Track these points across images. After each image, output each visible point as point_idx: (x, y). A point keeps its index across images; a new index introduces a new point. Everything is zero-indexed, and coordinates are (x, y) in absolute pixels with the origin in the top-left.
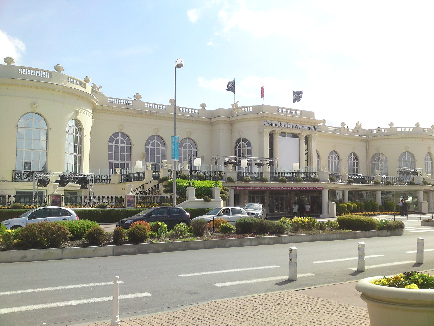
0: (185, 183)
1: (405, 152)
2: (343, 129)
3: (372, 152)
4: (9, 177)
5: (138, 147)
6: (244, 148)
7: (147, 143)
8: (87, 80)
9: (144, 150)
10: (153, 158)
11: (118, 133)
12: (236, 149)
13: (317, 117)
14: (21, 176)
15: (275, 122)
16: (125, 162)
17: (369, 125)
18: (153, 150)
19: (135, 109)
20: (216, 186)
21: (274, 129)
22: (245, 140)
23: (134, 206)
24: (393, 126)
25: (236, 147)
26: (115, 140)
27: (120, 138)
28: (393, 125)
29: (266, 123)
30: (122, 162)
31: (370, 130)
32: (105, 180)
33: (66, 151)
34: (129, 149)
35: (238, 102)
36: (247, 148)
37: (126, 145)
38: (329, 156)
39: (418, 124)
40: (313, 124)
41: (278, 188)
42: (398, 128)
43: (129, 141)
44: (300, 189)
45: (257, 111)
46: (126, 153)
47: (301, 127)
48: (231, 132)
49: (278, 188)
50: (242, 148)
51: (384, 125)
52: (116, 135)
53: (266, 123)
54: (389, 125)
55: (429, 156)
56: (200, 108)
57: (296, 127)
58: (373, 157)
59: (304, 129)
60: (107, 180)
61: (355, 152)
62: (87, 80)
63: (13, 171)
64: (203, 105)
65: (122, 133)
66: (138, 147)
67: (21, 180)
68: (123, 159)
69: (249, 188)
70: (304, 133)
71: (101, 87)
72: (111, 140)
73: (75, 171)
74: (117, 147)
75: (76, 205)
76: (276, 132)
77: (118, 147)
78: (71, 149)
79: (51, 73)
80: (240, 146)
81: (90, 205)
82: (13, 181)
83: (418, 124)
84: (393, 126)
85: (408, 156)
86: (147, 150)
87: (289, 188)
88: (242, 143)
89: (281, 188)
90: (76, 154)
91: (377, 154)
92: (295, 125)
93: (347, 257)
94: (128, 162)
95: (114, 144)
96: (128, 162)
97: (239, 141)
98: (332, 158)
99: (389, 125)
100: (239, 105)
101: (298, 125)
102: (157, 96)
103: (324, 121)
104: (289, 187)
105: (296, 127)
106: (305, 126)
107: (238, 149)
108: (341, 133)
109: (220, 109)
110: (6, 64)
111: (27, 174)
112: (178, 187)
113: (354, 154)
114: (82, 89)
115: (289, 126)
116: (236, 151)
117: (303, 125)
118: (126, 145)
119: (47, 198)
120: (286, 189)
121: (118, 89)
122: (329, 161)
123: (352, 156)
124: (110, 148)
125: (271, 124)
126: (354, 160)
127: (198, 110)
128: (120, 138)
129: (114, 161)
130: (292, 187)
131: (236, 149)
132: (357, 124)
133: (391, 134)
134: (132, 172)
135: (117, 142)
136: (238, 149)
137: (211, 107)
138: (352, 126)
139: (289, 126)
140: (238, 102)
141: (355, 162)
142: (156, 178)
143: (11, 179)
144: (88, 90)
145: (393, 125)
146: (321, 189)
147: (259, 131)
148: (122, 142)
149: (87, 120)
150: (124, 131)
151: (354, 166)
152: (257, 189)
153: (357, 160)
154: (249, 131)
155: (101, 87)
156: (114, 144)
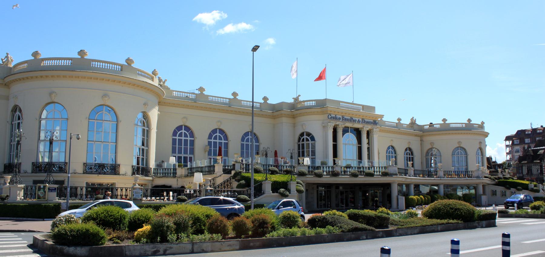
0: (259, 177)
2: (399, 125)
3: (427, 147)
4: (80, 169)
5: (201, 141)
6: (308, 142)
7: (210, 137)
8: (154, 73)
9: (207, 144)
10: (180, 149)
11: (216, 129)
13: (378, 112)
14: (91, 168)
15: (338, 116)
16: (188, 156)
17: (423, 121)
18: (180, 141)
19: (199, 101)
20: (266, 179)
21: (337, 123)
22: (309, 134)
23: (197, 196)
24: (446, 122)
25: (299, 141)
26: (179, 133)
27: (218, 134)
28: (446, 120)
29: (330, 117)
30: (186, 155)
31: (424, 126)
32: (165, 173)
33: (135, 144)
34: (192, 143)
35: (299, 96)
37: (189, 139)
38: (387, 151)
39: (469, 120)
40: (374, 119)
45: (322, 104)
46: (189, 147)
47: (364, 121)
48: (294, 125)
50: (305, 142)
51: (437, 121)
52: (179, 128)
53: (330, 117)
54: (443, 120)
55: (479, 151)
56: (263, 101)
57: (359, 121)
58: (427, 153)
59: (359, 127)
60: (168, 173)
62: (154, 73)
63: (84, 164)
66: (201, 141)
67: (91, 173)
68: (186, 152)
70: (367, 128)
71: (166, 80)
72: (175, 134)
73: (138, 164)
74: (215, 143)
75: (76, 197)
77: (182, 140)
78: (139, 143)
79: (122, 66)
81: (81, 197)
82: (84, 173)
83: (469, 120)
84: (446, 122)
85: (461, 150)
88: (305, 137)
90: (143, 147)
91: (431, 149)
92: (357, 119)
93: (531, 240)
94: (191, 156)
96: (191, 156)
97: (302, 135)
99: (443, 120)
100: (301, 99)
101: (361, 120)
102: (219, 90)
103: (382, 116)
105: (359, 121)
106: (367, 120)
107: (301, 143)
108: (397, 128)
109: (282, 102)
110: (80, 57)
111: (100, 169)
112: (256, 181)
113: (410, 149)
114: (150, 82)
115: (351, 120)
116: (299, 145)
118: (189, 139)
119: (128, 190)
121: (181, 82)
123: (408, 151)
124: (174, 141)
125: (335, 118)
126: (392, 153)
127: (260, 103)
128: (218, 134)
132: (412, 119)
133: (446, 129)
134: (194, 166)
135: (215, 138)
136: (301, 143)
137: (273, 101)
138: (406, 121)
139: (351, 120)
140: (299, 96)
141: (411, 156)
142: (226, 171)
143: (82, 172)
144: (156, 83)
145: (446, 120)
147: (323, 125)
148: (186, 136)
149: (154, 115)
150: (221, 128)
153: (412, 155)
154: (314, 125)
155: (166, 80)
156: (177, 138)
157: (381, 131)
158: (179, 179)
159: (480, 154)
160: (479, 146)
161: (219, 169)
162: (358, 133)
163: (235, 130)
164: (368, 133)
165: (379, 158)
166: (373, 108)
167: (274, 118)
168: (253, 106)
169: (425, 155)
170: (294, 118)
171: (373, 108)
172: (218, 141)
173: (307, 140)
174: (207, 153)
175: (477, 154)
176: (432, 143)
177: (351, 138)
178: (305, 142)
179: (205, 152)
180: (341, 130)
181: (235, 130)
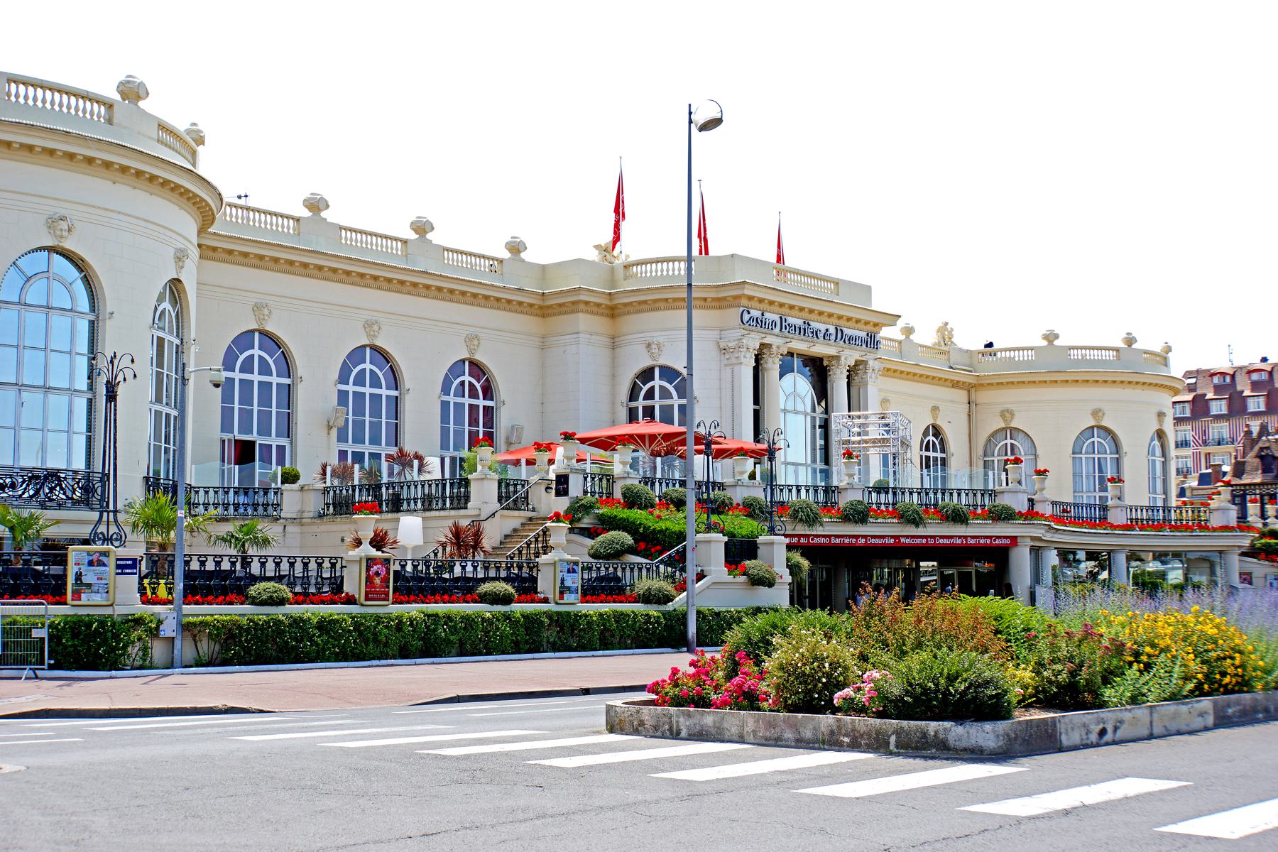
1: (1092, 428)
12: (633, 404)
24: (1056, 343)
26: (242, 357)
28: (1057, 336)
29: (746, 317)
34: (288, 393)
36: (676, 402)
37: (275, 380)
41: (892, 541)
42: (1071, 348)
43: (287, 366)
44: (945, 541)
49: (892, 541)
50: (657, 402)
53: (746, 317)
54: (1046, 337)
55: (1156, 442)
59: (825, 349)
61: (939, 422)
64: (516, 248)
65: (376, 349)
68: (359, 439)
69: (803, 540)
70: (850, 356)
76: (774, 349)
79: (1117, 350)
80: (650, 395)
86: (343, 396)
87: (924, 541)
88: (657, 382)
89: (903, 540)
92: (822, 327)
95: (237, 375)
97: (647, 375)
98: (247, 367)
99: (1046, 337)
101: (832, 330)
104: (926, 537)
107: (641, 403)
113: (477, 369)
117: (846, 331)
118: (275, 380)
120: (917, 541)
122: (445, 405)
123: (931, 438)
127: (405, 242)
129: (350, 448)
130: (934, 537)
131: (633, 404)
135: (247, 367)
136: (641, 403)
139: (803, 331)
145: (1057, 336)
146: (1008, 542)
148: (665, 394)
151: (473, 421)
152: (827, 541)
157: (889, 372)
158: (290, 529)
159: (1158, 451)
160: (1156, 427)
161: (484, 494)
162: (819, 371)
163: (429, 351)
164: (852, 373)
165: (71, 412)
166: (868, 289)
167: (544, 316)
168: (690, 285)
169: (981, 452)
170: (613, 316)
171: (868, 289)
172: (256, 377)
173: (665, 394)
174: (334, 432)
175: (1151, 452)
176: (1006, 414)
177: (801, 384)
178: (657, 402)
179: (330, 428)
180: (778, 363)
181: (429, 351)
